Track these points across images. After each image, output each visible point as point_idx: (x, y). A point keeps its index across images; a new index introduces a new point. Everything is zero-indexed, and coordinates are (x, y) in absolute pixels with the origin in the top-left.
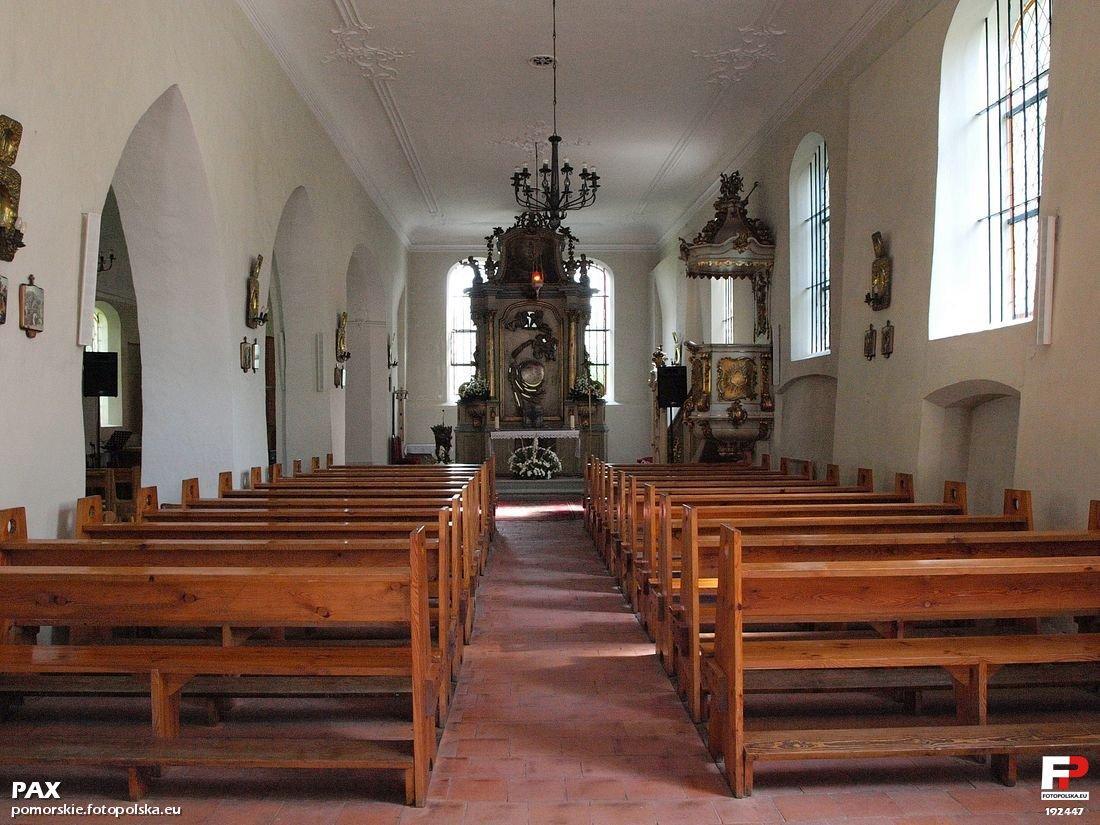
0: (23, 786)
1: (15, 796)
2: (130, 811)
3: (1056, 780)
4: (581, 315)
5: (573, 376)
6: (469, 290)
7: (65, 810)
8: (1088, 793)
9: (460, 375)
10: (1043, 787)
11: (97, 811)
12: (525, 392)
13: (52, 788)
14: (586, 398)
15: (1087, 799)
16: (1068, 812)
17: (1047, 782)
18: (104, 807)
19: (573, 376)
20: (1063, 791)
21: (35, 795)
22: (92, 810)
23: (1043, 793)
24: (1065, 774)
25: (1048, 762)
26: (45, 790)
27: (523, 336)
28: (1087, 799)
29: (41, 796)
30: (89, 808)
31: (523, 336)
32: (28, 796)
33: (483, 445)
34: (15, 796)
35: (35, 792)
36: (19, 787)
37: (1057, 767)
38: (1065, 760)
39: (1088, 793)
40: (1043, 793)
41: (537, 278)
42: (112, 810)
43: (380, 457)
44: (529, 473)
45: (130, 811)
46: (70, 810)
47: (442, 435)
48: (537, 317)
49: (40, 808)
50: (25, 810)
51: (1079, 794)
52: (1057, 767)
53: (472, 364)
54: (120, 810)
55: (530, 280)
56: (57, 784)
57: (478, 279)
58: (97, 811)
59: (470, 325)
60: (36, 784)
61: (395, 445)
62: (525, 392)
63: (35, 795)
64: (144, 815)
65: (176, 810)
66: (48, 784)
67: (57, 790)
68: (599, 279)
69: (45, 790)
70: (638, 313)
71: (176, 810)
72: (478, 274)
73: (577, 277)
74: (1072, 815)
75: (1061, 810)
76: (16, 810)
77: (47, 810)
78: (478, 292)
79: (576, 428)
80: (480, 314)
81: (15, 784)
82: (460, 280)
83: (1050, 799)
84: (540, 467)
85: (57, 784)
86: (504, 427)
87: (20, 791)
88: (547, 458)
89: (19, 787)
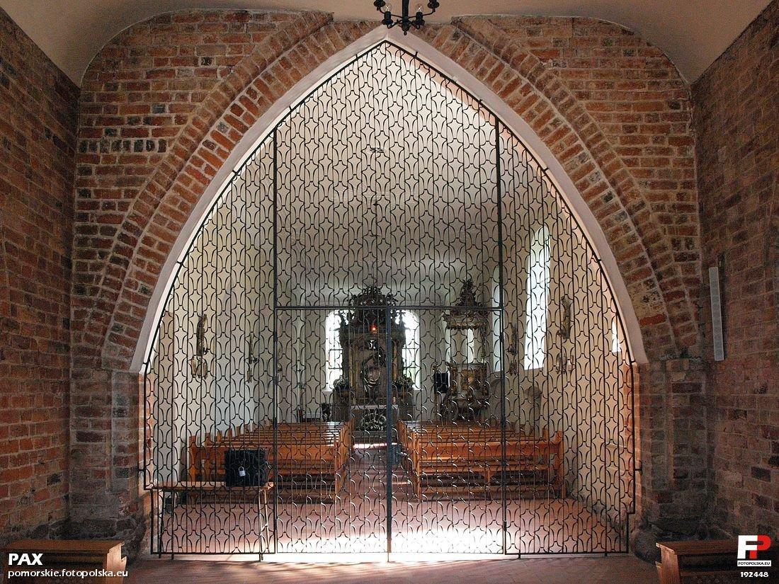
0: (17, 556)
1: (10, 563)
2: (92, 574)
3: (748, 553)
4: (399, 341)
5: (395, 375)
6: (339, 329)
7: (46, 573)
8: (770, 561)
9: (333, 375)
10: (738, 558)
11: (69, 574)
12: (369, 384)
13: (37, 559)
14: (406, 384)
15: (770, 565)
16: (756, 575)
17: (741, 554)
18: (73, 571)
19: (395, 375)
20: (763, 560)
21: (24, 563)
22: (65, 573)
23: (738, 561)
24: (754, 548)
25: (742, 540)
26: (32, 559)
27: (367, 354)
28: (770, 565)
29: (29, 563)
30: (63, 572)
31: (367, 354)
32: (20, 563)
33: (347, 413)
34: (10, 563)
35: (25, 560)
36: (14, 557)
37: (748, 543)
38: (754, 538)
39: (770, 561)
40: (738, 561)
41: (374, 329)
42: (79, 574)
43: (292, 419)
44: (372, 427)
45: (92, 574)
46: (50, 574)
47: (325, 407)
48: (376, 344)
49: (28, 572)
50: (18, 574)
51: (764, 562)
52: (748, 543)
53: (340, 368)
54: (85, 574)
55: (371, 323)
56: (40, 555)
57: (343, 324)
58: (69, 574)
59: (338, 346)
60: (25, 555)
61: (300, 412)
62: (369, 384)
63: (24, 563)
64: (102, 577)
65: (125, 574)
66: (34, 555)
67: (40, 559)
68: (410, 321)
69: (32, 559)
70: (430, 343)
71: (125, 574)
72: (343, 320)
73: (397, 321)
74: (759, 577)
75: (751, 573)
76: (11, 574)
77: (33, 574)
78: (343, 330)
79: (397, 404)
80: (344, 341)
81: (11, 555)
82: (333, 323)
83: (743, 565)
84: (377, 424)
85: (40, 555)
86: (360, 402)
87: (14, 560)
88: (381, 420)
89: (14, 557)
